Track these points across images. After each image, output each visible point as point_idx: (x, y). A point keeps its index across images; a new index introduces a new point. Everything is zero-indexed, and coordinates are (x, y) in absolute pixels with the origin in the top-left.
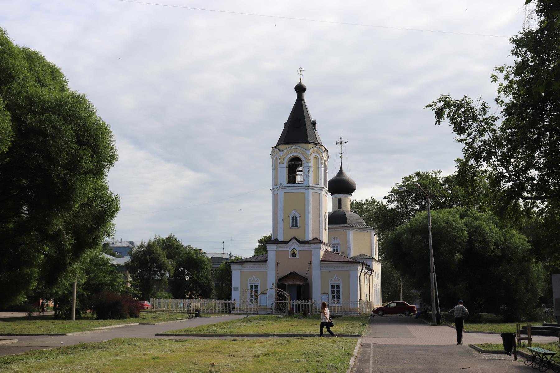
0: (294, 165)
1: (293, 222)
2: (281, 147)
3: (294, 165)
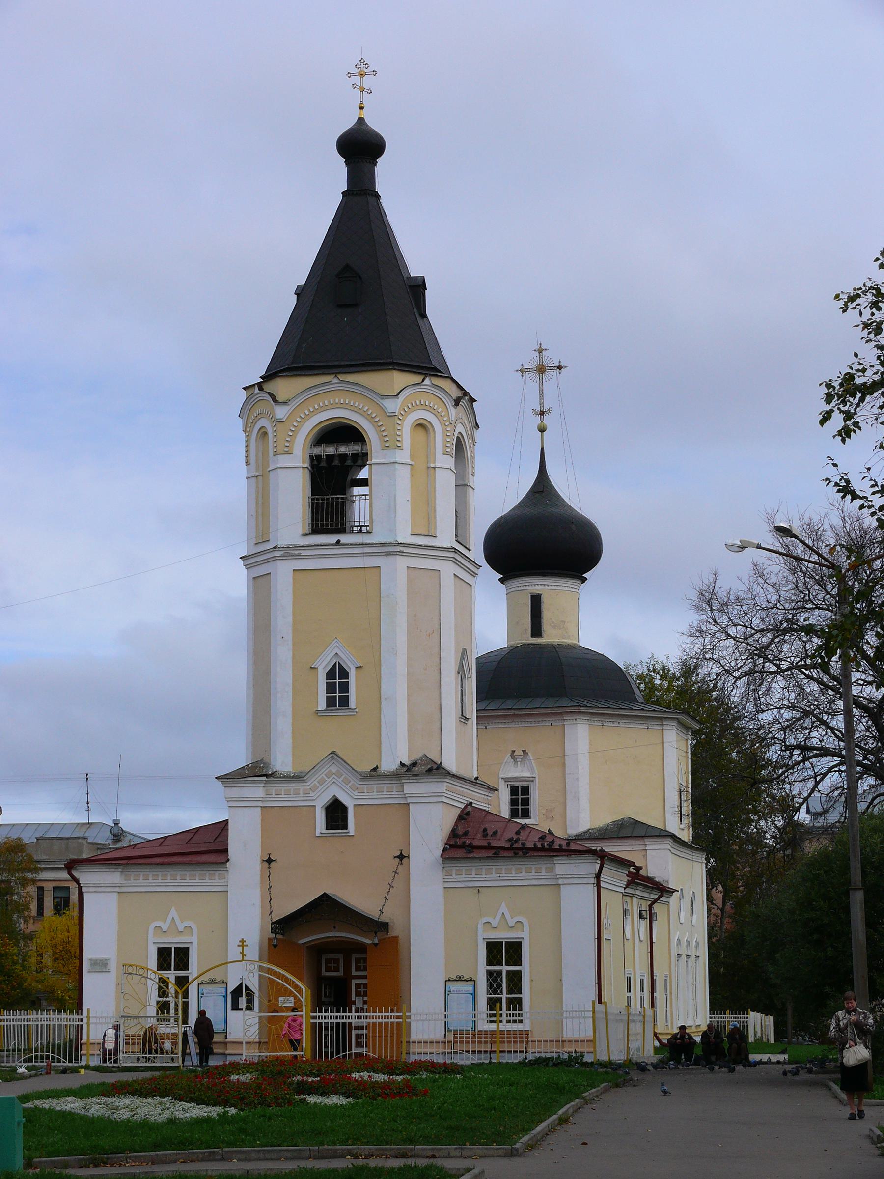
0: (335, 473)
1: (330, 688)
2: (284, 387)
3: (335, 473)
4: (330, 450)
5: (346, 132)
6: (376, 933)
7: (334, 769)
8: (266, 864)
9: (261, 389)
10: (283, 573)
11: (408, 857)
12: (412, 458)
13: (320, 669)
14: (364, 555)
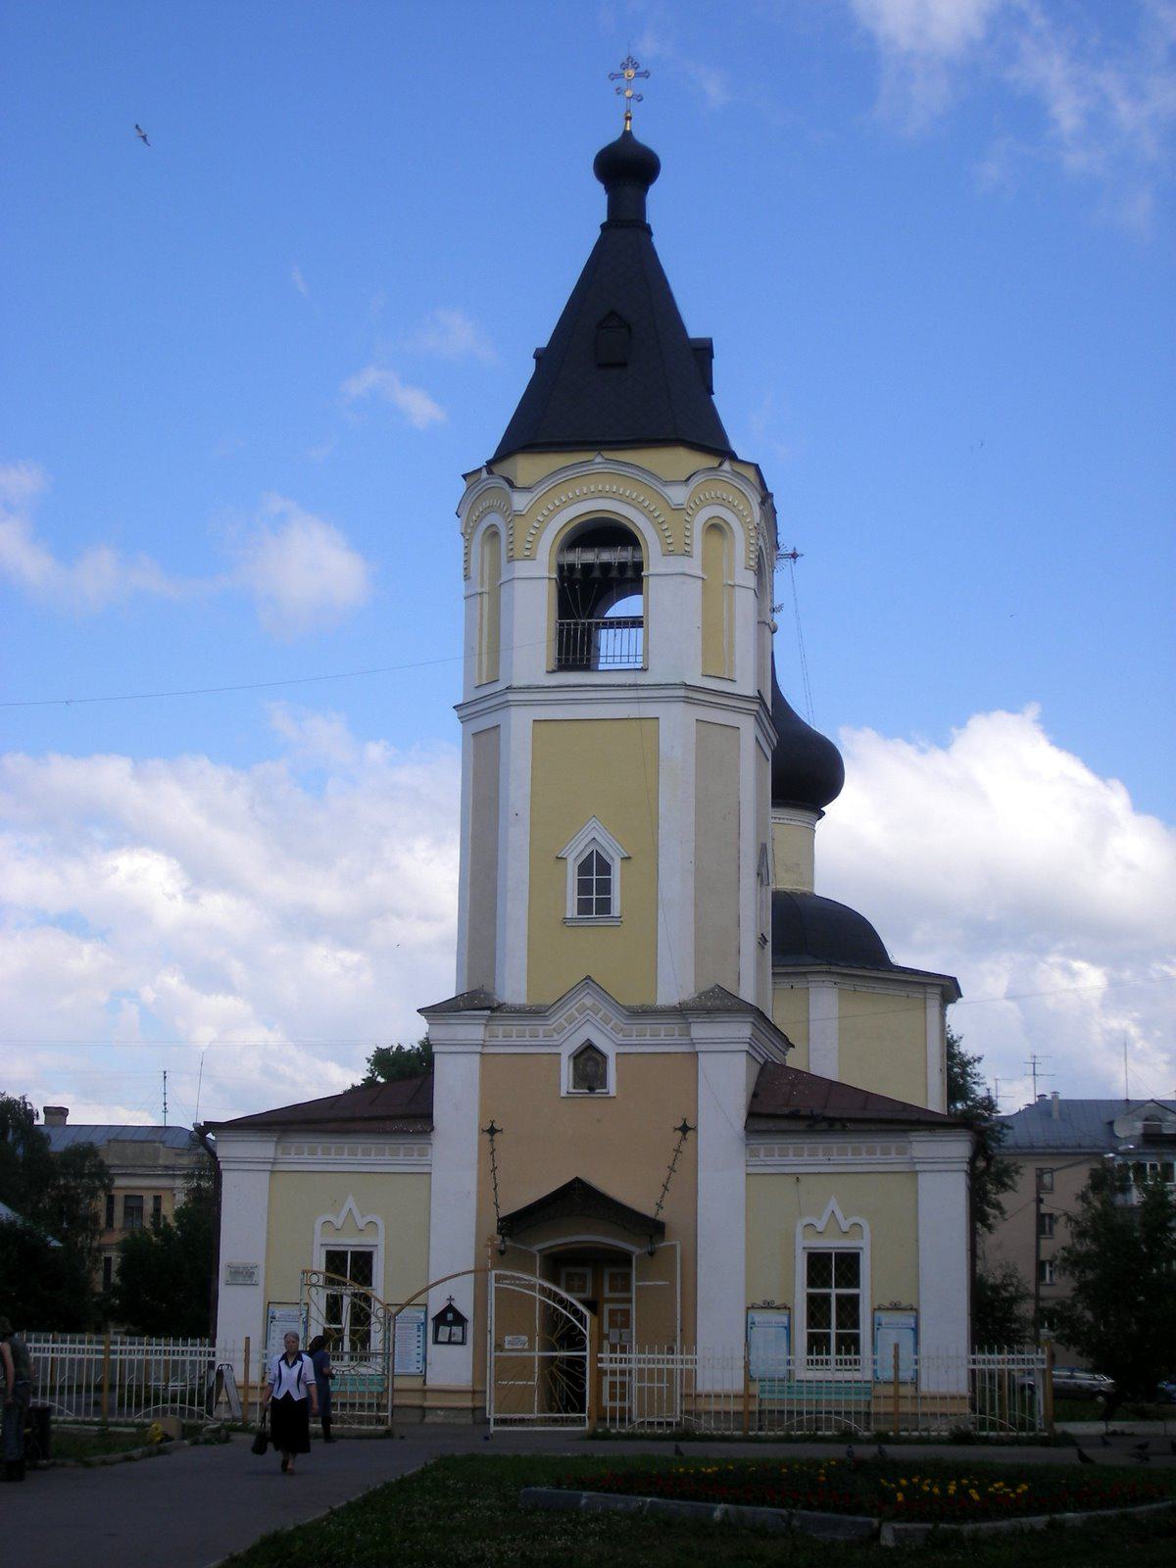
0: (596, 580)
1: (584, 887)
2: (527, 467)
3: (596, 580)
4: (590, 557)
5: (610, 145)
6: (651, 1237)
7: (588, 1001)
8: (487, 1136)
9: (490, 472)
10: (519, 724)
11: (695, 1129)
12: (704, 568)
13: (570, 860)
14: (639, 700)
